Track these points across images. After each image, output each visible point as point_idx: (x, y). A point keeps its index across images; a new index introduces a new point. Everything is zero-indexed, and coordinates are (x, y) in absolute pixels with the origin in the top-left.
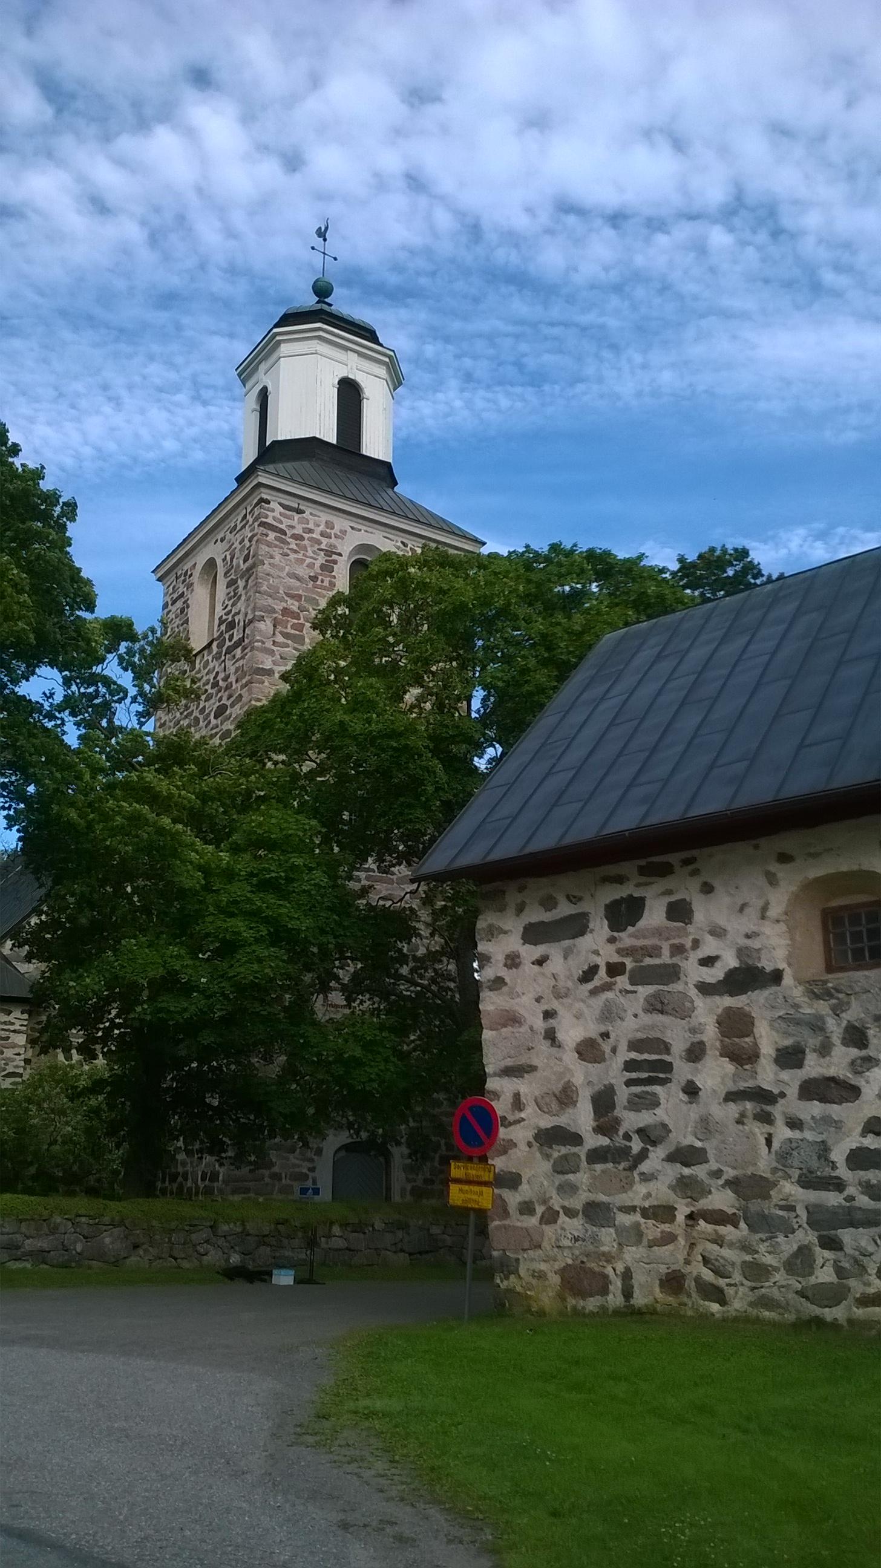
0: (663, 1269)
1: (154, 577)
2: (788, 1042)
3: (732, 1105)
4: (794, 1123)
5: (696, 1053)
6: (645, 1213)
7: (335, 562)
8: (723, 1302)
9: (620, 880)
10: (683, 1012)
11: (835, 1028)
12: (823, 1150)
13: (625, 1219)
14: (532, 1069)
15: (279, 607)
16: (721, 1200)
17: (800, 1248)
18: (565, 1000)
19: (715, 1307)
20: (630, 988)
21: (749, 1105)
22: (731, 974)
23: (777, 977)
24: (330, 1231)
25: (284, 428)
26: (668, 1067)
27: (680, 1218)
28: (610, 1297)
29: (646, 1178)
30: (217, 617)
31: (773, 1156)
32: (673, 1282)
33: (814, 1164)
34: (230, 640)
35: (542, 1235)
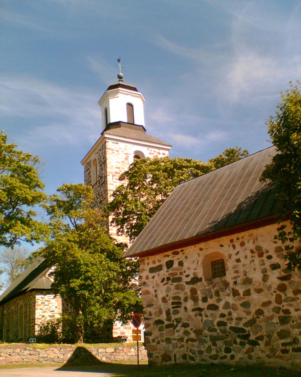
0: (182, 354)
1: (81, 164)
2: (204, 296)
3: (194, 312)
4: (206, 316)
5: (186, 299)
6: (178, 340)
7: (128, 157)
8: (194, 360)
9: (168, 256)
10: (183, 289)
11: (213, 291)
12: (212, 322)
13: (174, 342)
14: (153, 305)
15: (114, 171)
16: (193, 335)
17: (209, 346)
18: (158, 287)
19: (193, 362)
20: (171, 283)
21: (197, 312)
22: (192, 279)
23: (201, 279)
24: (130, 350)
25: (113, 119)
26: (180, 303)
27: (185, 341)
28: (172, 361)
29: (178, 331)
30: (98, 175)
31: (203, 324)
32: (184, 356)
33: (211, 326)
34: (102, 181)
35: (157, 347)
